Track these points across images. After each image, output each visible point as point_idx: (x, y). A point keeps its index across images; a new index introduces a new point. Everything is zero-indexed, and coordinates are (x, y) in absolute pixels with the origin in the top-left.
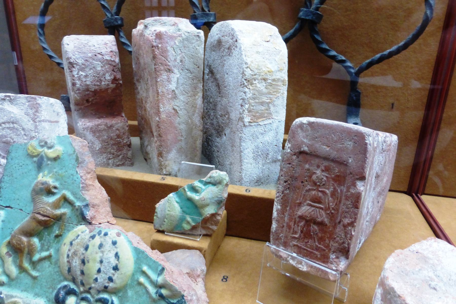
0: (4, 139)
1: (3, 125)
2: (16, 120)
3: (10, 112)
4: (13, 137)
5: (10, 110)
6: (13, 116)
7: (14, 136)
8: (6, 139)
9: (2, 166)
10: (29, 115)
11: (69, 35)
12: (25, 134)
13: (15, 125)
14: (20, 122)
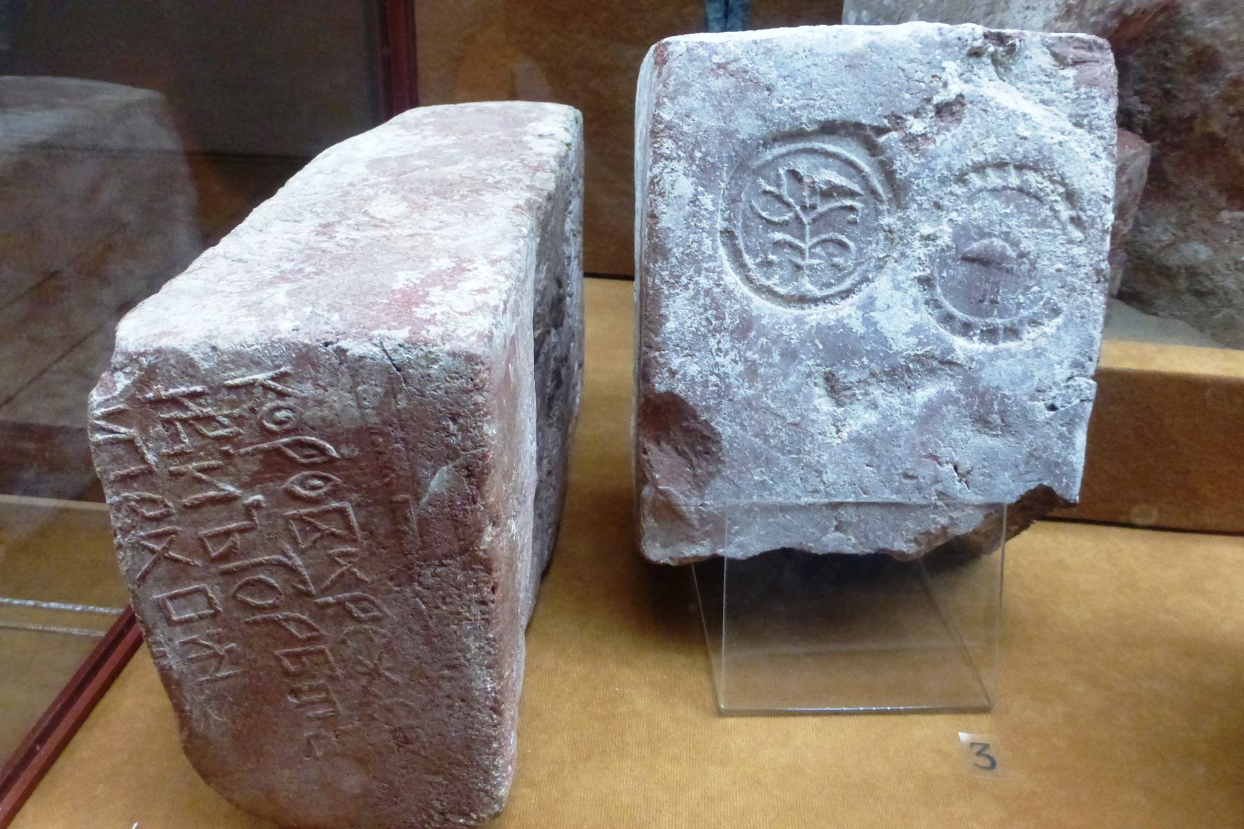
0: (975, 245)
1: (975, 180)
2: (1040, 151)
3: (1014, 112)
4: (1016, 234)
5: (1011, 106)
6: (1026, 134)
7: (1024, 230)
8: (986, 241)
9: (960, 366)
10: (1098, 128)
11: (282, 185)
12: (1076, 221)
13: (1032, 178)
14: (1060, 161)
